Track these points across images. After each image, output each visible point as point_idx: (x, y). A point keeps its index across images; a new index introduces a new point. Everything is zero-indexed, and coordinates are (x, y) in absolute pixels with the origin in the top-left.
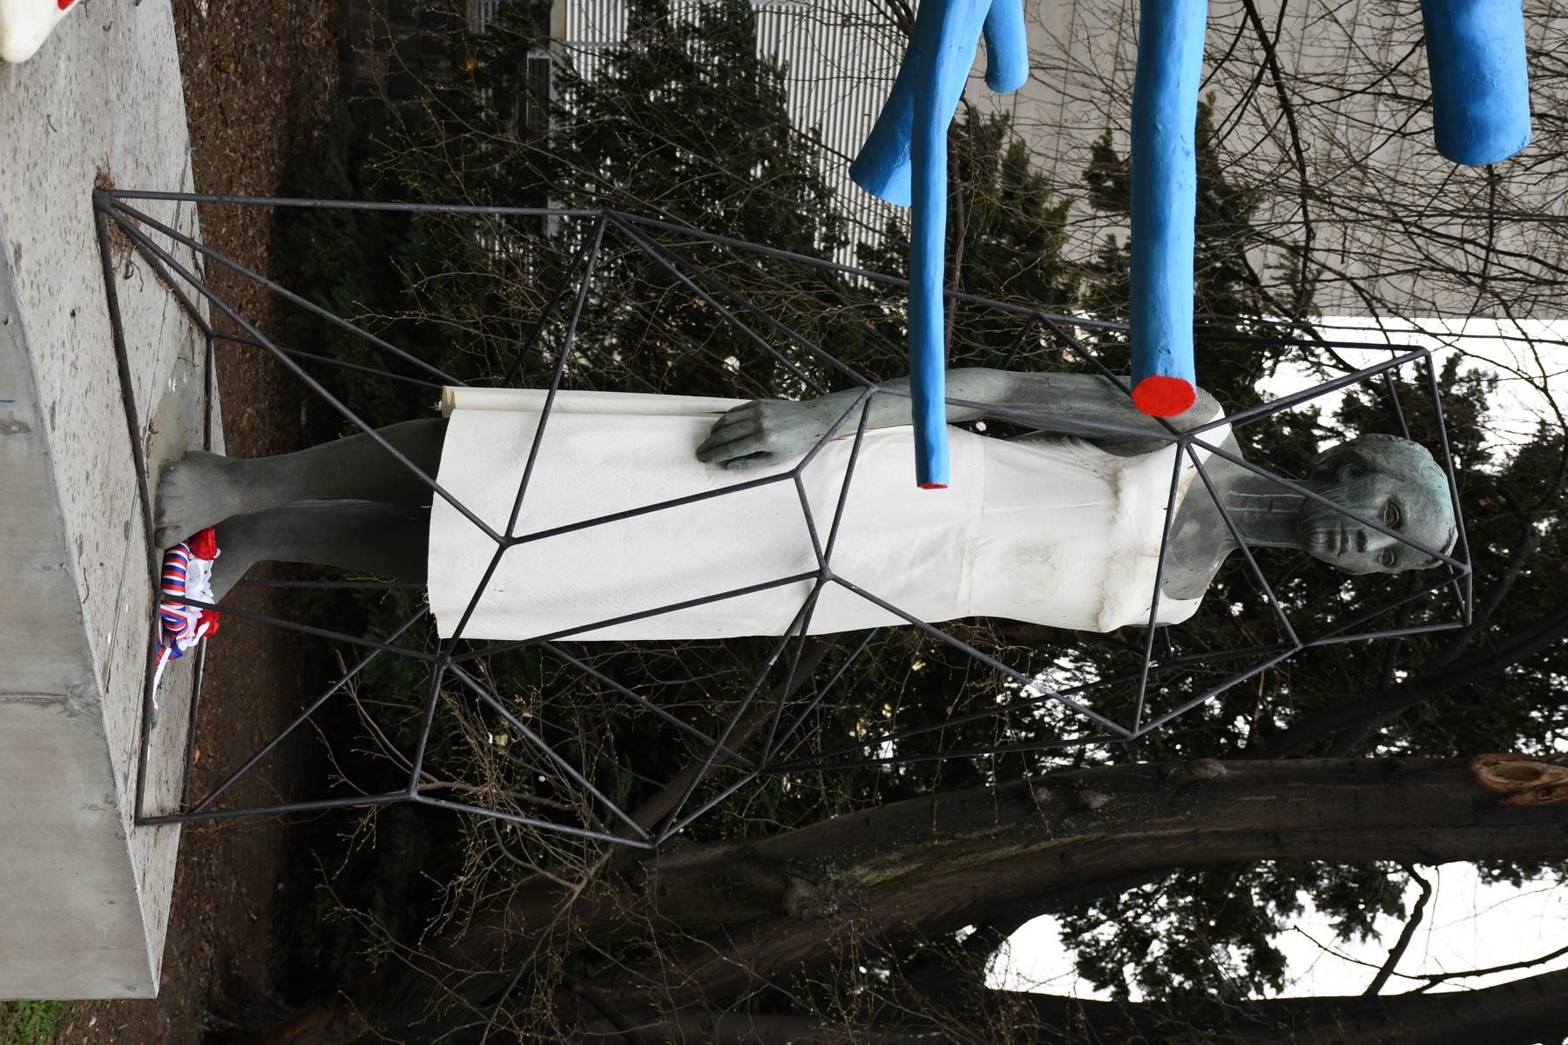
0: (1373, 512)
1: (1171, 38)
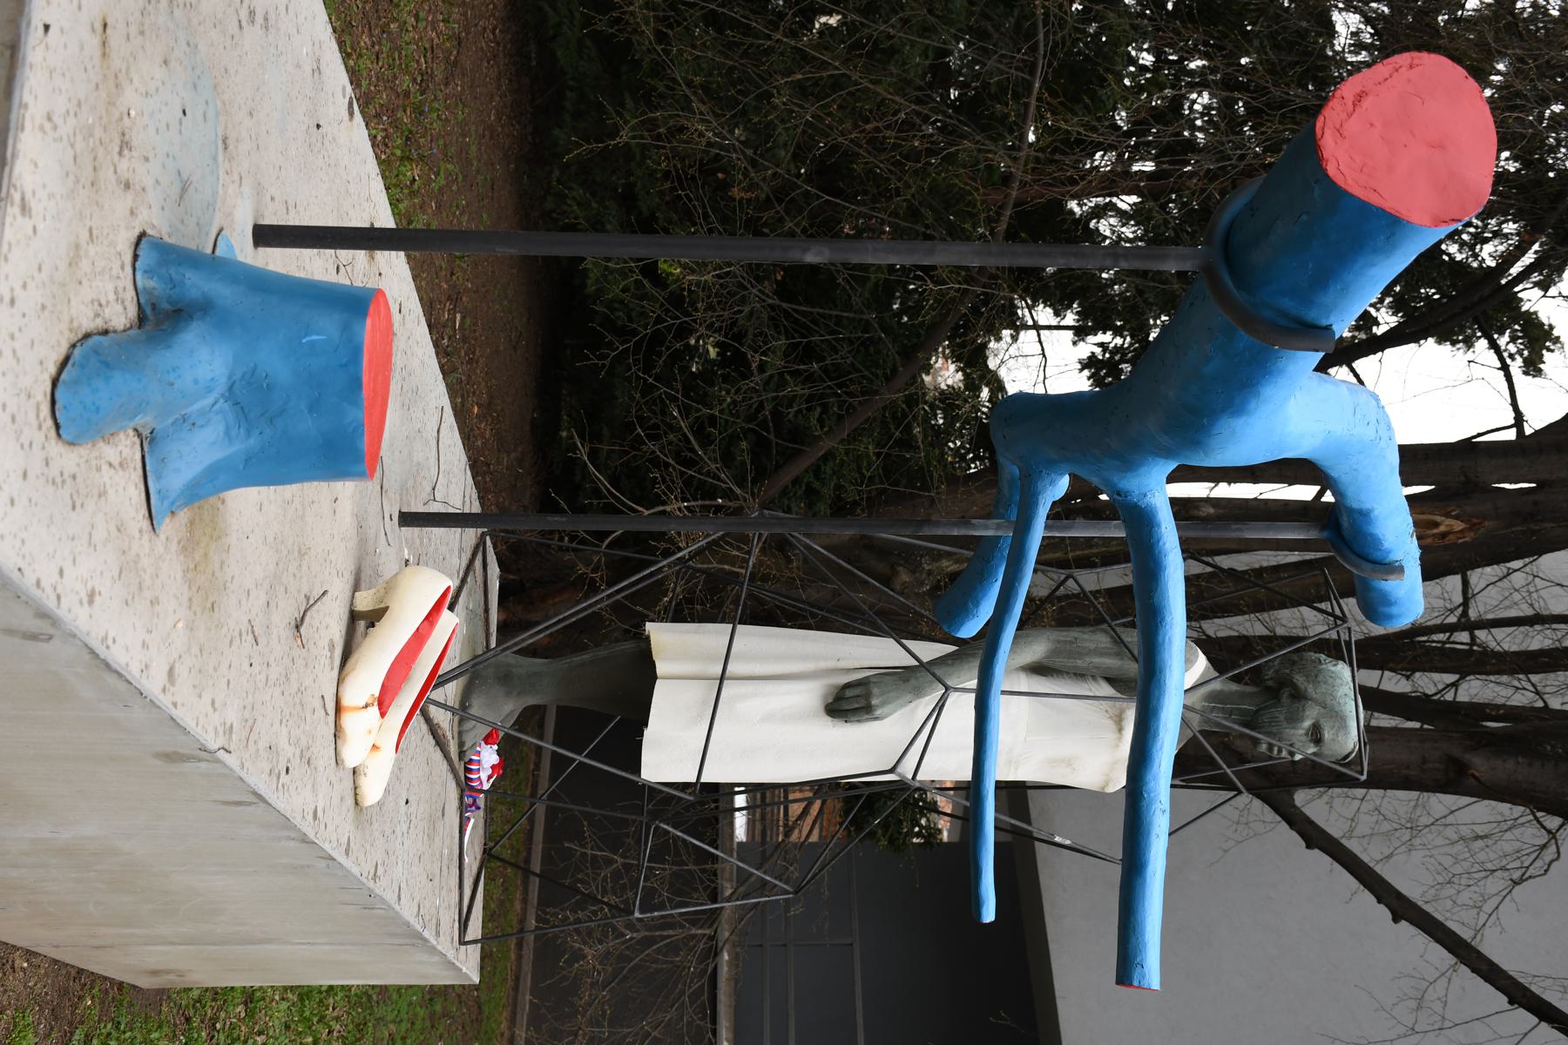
0: (1302, 732)
1: (1156, 735)
